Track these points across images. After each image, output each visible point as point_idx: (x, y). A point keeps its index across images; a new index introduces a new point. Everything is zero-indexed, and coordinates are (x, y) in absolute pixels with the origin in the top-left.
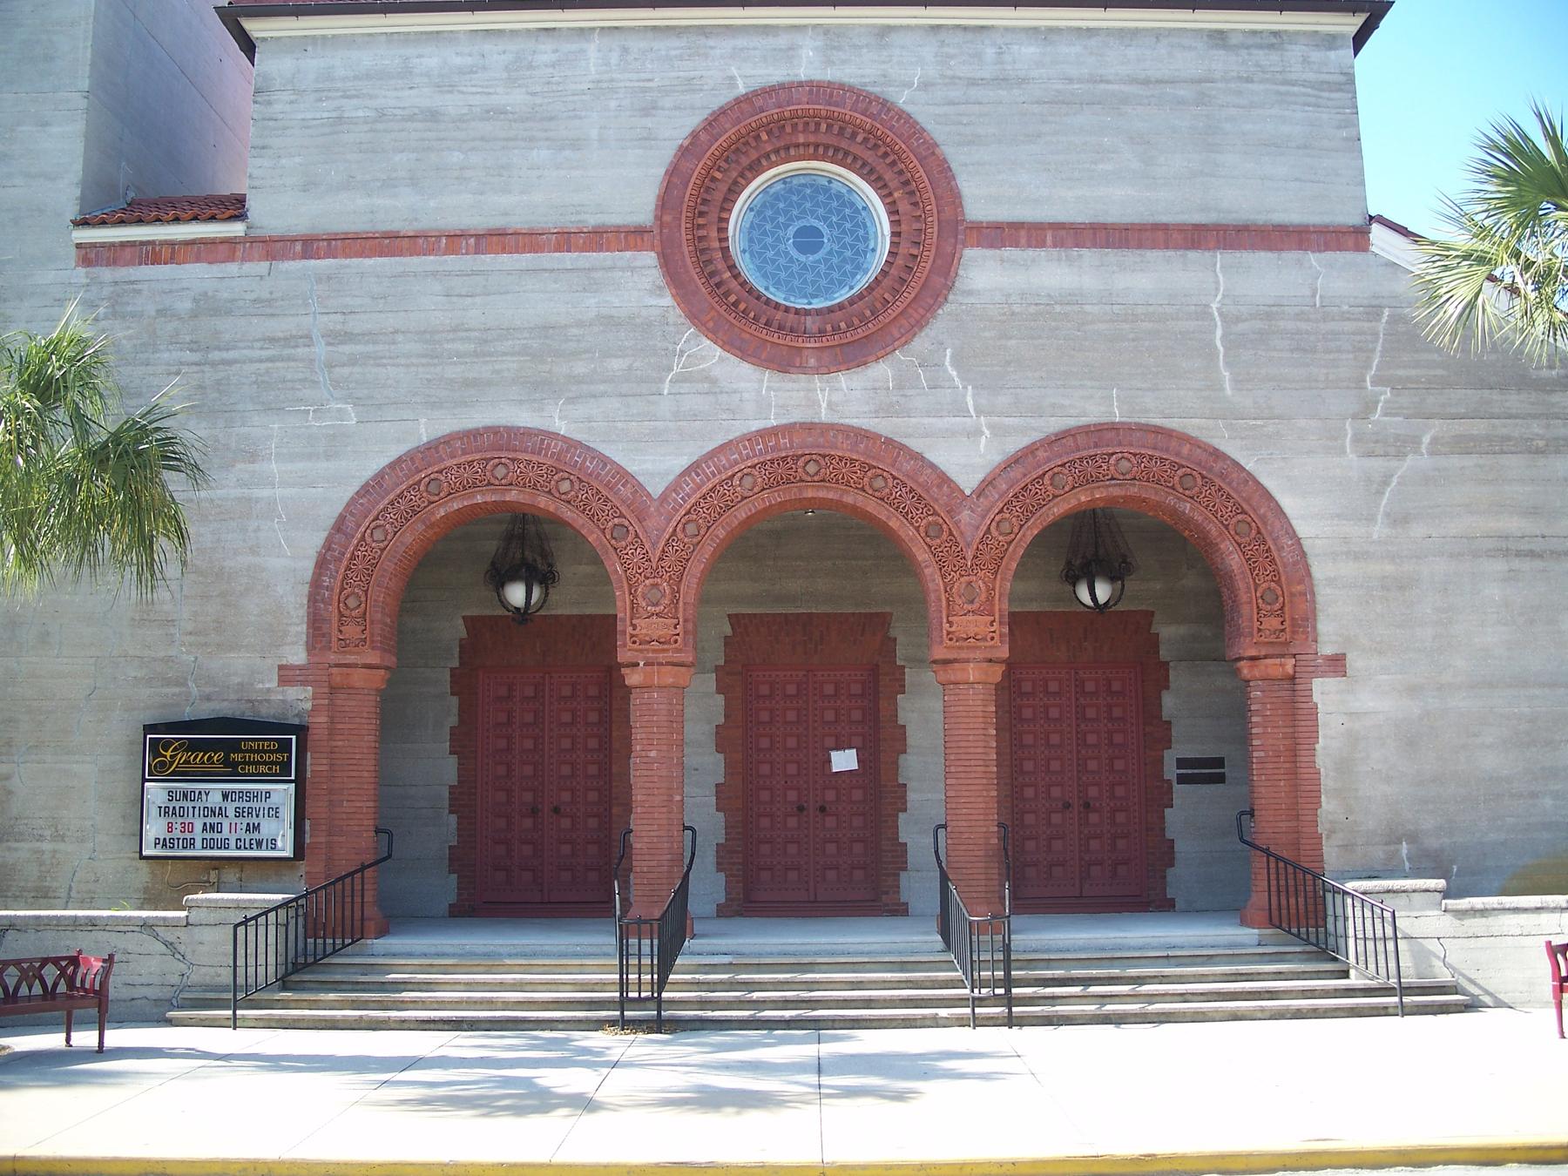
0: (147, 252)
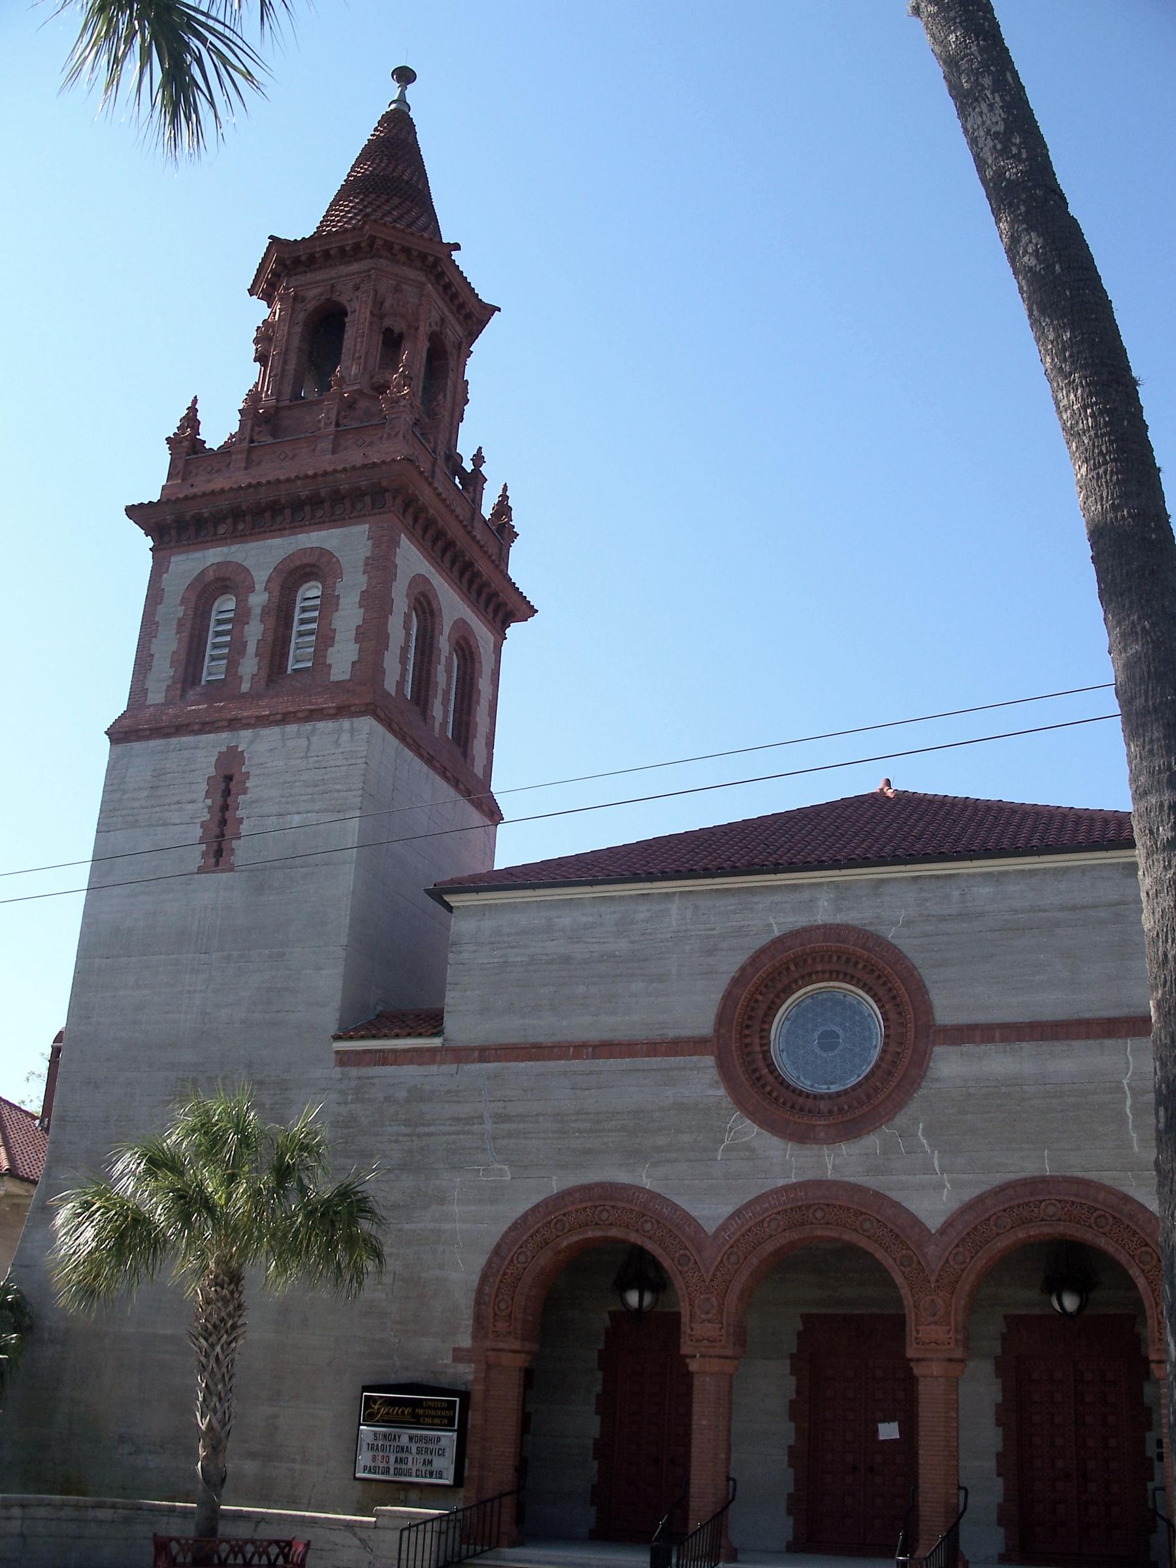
0: (379, 1057)
